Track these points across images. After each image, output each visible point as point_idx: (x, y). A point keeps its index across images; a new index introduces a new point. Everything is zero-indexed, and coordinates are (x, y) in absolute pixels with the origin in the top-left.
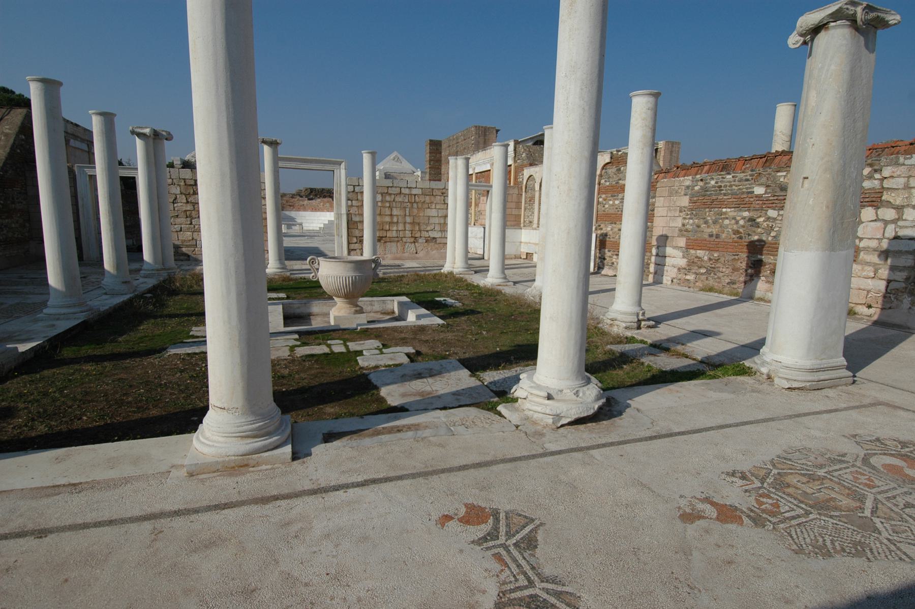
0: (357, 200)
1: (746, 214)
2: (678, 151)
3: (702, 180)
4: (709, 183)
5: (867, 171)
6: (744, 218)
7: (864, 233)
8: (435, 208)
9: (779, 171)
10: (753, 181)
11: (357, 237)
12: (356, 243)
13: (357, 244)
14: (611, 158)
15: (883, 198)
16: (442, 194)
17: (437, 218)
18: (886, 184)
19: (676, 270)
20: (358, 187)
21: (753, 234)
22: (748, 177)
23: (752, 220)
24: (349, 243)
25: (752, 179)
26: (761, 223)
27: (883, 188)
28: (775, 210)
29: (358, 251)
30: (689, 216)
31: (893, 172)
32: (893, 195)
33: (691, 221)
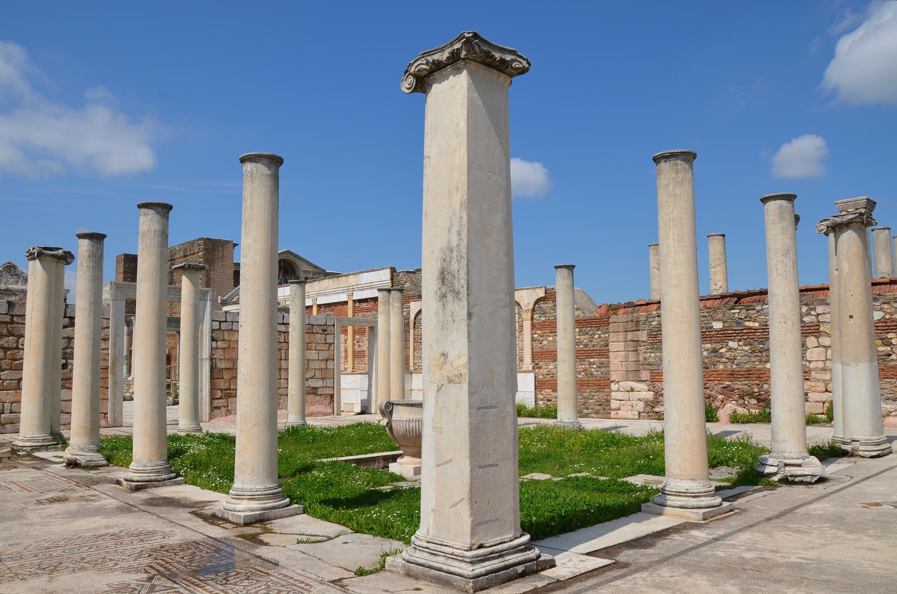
1: (708, 346)
2: (183, 244)
5: (804, 309)
6: (707, 350)
7: (811, 358)
9: (732, 309)
10: (710, 318)
11: (221, 390)
12: (219, 399)
14: (546, 293)
15: (821, 329)
16: (323, 331)
18: (821, 318)
19: (642, 404)
20: (225, 323)
21: (718, 364)
22: (705, 314)
23: (715, 351)
24: (212, 398)
25: (709, 316)
26: (724, 353)
27: (819, 322)
28: (734, 341)
29: (223, 409)
30: (650, 350)
31: (825, 310)
32: (827, 327)
33: (653, 355)
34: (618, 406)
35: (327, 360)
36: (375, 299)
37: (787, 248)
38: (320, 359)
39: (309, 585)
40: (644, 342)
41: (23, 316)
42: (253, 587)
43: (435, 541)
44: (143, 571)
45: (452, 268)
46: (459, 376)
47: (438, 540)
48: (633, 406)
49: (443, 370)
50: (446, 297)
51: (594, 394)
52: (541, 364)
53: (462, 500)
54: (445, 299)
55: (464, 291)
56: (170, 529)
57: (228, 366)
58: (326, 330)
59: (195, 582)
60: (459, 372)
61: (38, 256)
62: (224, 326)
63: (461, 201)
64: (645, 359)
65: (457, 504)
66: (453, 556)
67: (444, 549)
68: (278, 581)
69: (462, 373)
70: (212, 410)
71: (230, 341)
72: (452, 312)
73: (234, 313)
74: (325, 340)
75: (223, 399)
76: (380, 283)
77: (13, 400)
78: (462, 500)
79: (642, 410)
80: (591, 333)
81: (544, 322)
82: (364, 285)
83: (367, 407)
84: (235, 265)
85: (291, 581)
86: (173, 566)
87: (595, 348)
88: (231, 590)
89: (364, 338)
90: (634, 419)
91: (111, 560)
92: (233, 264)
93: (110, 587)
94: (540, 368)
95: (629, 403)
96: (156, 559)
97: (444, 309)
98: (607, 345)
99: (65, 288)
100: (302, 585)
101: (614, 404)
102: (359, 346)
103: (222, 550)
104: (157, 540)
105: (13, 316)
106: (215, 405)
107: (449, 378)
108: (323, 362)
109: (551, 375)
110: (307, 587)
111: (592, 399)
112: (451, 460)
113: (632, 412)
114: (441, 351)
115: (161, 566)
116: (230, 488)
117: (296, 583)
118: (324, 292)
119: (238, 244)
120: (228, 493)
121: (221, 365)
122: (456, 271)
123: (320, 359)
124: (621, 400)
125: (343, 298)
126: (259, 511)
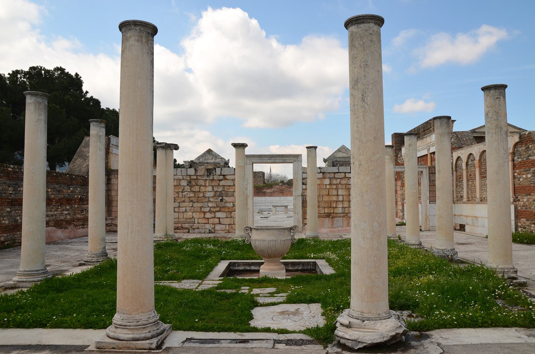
37: (356, 79)
52: (519, 197)
81: (521, 162)
94: (519, 200)
105: (197, 176)
109: (525, 207)
119: (456, 120)
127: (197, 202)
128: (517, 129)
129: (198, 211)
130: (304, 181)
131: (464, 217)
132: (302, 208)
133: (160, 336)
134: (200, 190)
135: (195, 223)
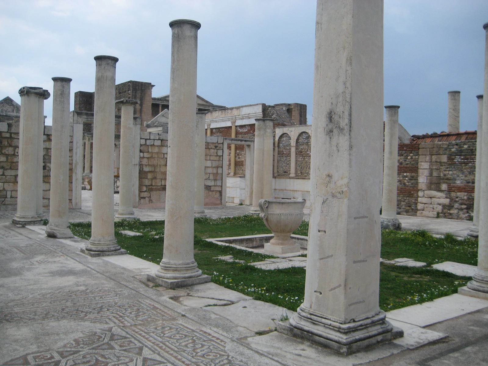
0: (148, 152)
3: (457, 145)
4: (463, 147)
8: (210, 160)
11: (146, 186)
12: (145, 192)
13: (146, 193)
17: (211, 168)
29: (147, 198)
30: (448, 169)
33: (451, 172)
34: (422, 208)
35: (217, 167)
36: (252, 126)
38: (213, 166)
39: (224, 341)
40: (444, 163)
41: (18, 133)
42: (183, 340)
43: (316, 314)
44: (104, 322)
45: (338, 110)
46: (341, 193)
47: (319, 314)
48: (433, 208)
49: (328, 187)
50: (332, 132)
51: (405, 198)
53: (340, 286)
54: (331, 134)
55: (347, 128)
56: (120, 290)
57: (151, 170)
58: (217, 147)
59: (142, 334)
60: (341, 190)
61: (26, 93)
62: (148, 142)
63: (347, 58)
64: (445, 175)
65: (335, 288)
66: (331, 327)
67: (324, 320)
68: (200, 337)
69: (344, 191)
70: (140, 199)
71: (152, 153)
72: (337, 144)
73: (155, 133)
74: (217, 153)
75: (147, 192)
76: (255, 114)
77: (12, 189)
78: (340, 286)
79: (440, 212)
80: (405, 155)
82: (243, 116)
83: (244, 200)
84: (153, 100)
85: (210, 337)
86: (125, 320)
87: (408, 166)
88: (168, 342)
89: (242, 153)
90: (434, 217)
91: (82, 312)
92: (151, 99)
93: (83, 334)
95: (431, 206)
96: (113, 313)
97: (330, 141)
98: (417, 163)
99: (44, 115)
100: (218, 341)
101: (420, 206)
102: (239, 158)
103: (158, 308)
104: (111, 297)
106: (142, 196)
107: (333, 194)
108: (215, 169)
110: (222, 343)
111: (404, 202)
112: (332, 256)
113: (433, 212)
114: (326, 173)
115: (117, 318)
116: (160, 261)
117: (213, 339)
118: (215, 120)
120: (158, 263)
121: (146, 169)
122: (342, 112)
123: (213, 166)
124: (425, 204)
125: (229, 124)
126: (181, 279)
127: (11, 169)
128: (204, 101)
129: (12, 181)
130: (142, 148)
131: (289, 191)
132: (139, 179)
133: (308, 324)
134: (14, 153)
135: (6, 197)
